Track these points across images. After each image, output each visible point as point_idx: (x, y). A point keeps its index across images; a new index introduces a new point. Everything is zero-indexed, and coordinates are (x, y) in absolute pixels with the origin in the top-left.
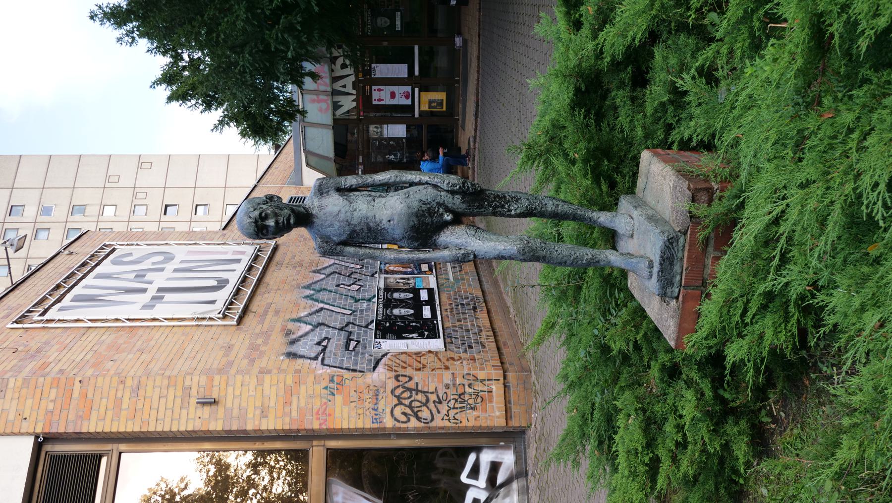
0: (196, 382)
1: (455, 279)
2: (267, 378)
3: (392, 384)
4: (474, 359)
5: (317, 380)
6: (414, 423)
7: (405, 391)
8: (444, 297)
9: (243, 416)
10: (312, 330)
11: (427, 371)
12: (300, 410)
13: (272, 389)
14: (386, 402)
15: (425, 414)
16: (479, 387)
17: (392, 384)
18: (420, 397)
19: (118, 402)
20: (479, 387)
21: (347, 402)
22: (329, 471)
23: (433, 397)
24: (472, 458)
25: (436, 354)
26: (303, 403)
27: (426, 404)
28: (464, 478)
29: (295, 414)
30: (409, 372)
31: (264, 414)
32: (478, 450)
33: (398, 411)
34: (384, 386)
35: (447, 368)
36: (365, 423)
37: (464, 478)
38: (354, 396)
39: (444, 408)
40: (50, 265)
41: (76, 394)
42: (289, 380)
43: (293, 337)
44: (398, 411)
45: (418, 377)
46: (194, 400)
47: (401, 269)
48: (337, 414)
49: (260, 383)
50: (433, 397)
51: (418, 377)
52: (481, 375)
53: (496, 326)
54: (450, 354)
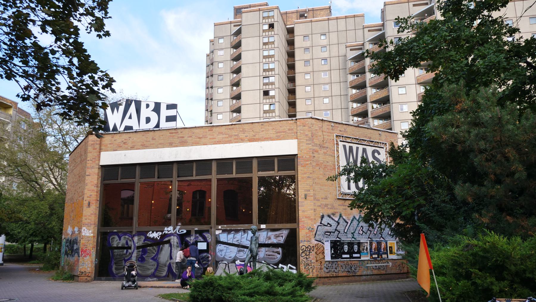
0: (311, 193)
1: (368, 267)
2: (313, 211)
3: (311, 245)
4: (321, 269)
5: (312, 225)
6: (301, 251)
7: (309, 249)
8: (356, 262)
9: (302, 206)
10: (335, 221)
11: (315, 255)
12: (304, 221)
13: (310, 213)
14: (306, 244)
15: (303, 255)
16: (311, 270)
17: (311, 245)
18: (308, 253)
19: (305, 173)
20: (311, 270)
21: (306, 233)
22: (290, 229)
23: (308, 257)
24: (294, 268)
25: (324, 258)
26: (306, 221)
27: (306, 255)
28: (289, 265)
29: (303, 220)
30: (315, 250)
31: (303, 211)
32: (296, 269)
33: (304, 247)
34: (311, 243)
35: (317, 261)
36: (301, 238)
37: (289, 265)
38: (308, 235)
39: (305, 260)
40: (372, 131)
41: (307, 162)
42: (312, 217)
43: (332, 216)
44: (304, 247)
45: (313, 253)
46: (306, 193)
47: (373, 247)
48: (303, 231)
49: (311, 209)
50: (308, 257)
51: (313, 253)
52: (314, 271)
53: (339, 278)
54: (323, 263)
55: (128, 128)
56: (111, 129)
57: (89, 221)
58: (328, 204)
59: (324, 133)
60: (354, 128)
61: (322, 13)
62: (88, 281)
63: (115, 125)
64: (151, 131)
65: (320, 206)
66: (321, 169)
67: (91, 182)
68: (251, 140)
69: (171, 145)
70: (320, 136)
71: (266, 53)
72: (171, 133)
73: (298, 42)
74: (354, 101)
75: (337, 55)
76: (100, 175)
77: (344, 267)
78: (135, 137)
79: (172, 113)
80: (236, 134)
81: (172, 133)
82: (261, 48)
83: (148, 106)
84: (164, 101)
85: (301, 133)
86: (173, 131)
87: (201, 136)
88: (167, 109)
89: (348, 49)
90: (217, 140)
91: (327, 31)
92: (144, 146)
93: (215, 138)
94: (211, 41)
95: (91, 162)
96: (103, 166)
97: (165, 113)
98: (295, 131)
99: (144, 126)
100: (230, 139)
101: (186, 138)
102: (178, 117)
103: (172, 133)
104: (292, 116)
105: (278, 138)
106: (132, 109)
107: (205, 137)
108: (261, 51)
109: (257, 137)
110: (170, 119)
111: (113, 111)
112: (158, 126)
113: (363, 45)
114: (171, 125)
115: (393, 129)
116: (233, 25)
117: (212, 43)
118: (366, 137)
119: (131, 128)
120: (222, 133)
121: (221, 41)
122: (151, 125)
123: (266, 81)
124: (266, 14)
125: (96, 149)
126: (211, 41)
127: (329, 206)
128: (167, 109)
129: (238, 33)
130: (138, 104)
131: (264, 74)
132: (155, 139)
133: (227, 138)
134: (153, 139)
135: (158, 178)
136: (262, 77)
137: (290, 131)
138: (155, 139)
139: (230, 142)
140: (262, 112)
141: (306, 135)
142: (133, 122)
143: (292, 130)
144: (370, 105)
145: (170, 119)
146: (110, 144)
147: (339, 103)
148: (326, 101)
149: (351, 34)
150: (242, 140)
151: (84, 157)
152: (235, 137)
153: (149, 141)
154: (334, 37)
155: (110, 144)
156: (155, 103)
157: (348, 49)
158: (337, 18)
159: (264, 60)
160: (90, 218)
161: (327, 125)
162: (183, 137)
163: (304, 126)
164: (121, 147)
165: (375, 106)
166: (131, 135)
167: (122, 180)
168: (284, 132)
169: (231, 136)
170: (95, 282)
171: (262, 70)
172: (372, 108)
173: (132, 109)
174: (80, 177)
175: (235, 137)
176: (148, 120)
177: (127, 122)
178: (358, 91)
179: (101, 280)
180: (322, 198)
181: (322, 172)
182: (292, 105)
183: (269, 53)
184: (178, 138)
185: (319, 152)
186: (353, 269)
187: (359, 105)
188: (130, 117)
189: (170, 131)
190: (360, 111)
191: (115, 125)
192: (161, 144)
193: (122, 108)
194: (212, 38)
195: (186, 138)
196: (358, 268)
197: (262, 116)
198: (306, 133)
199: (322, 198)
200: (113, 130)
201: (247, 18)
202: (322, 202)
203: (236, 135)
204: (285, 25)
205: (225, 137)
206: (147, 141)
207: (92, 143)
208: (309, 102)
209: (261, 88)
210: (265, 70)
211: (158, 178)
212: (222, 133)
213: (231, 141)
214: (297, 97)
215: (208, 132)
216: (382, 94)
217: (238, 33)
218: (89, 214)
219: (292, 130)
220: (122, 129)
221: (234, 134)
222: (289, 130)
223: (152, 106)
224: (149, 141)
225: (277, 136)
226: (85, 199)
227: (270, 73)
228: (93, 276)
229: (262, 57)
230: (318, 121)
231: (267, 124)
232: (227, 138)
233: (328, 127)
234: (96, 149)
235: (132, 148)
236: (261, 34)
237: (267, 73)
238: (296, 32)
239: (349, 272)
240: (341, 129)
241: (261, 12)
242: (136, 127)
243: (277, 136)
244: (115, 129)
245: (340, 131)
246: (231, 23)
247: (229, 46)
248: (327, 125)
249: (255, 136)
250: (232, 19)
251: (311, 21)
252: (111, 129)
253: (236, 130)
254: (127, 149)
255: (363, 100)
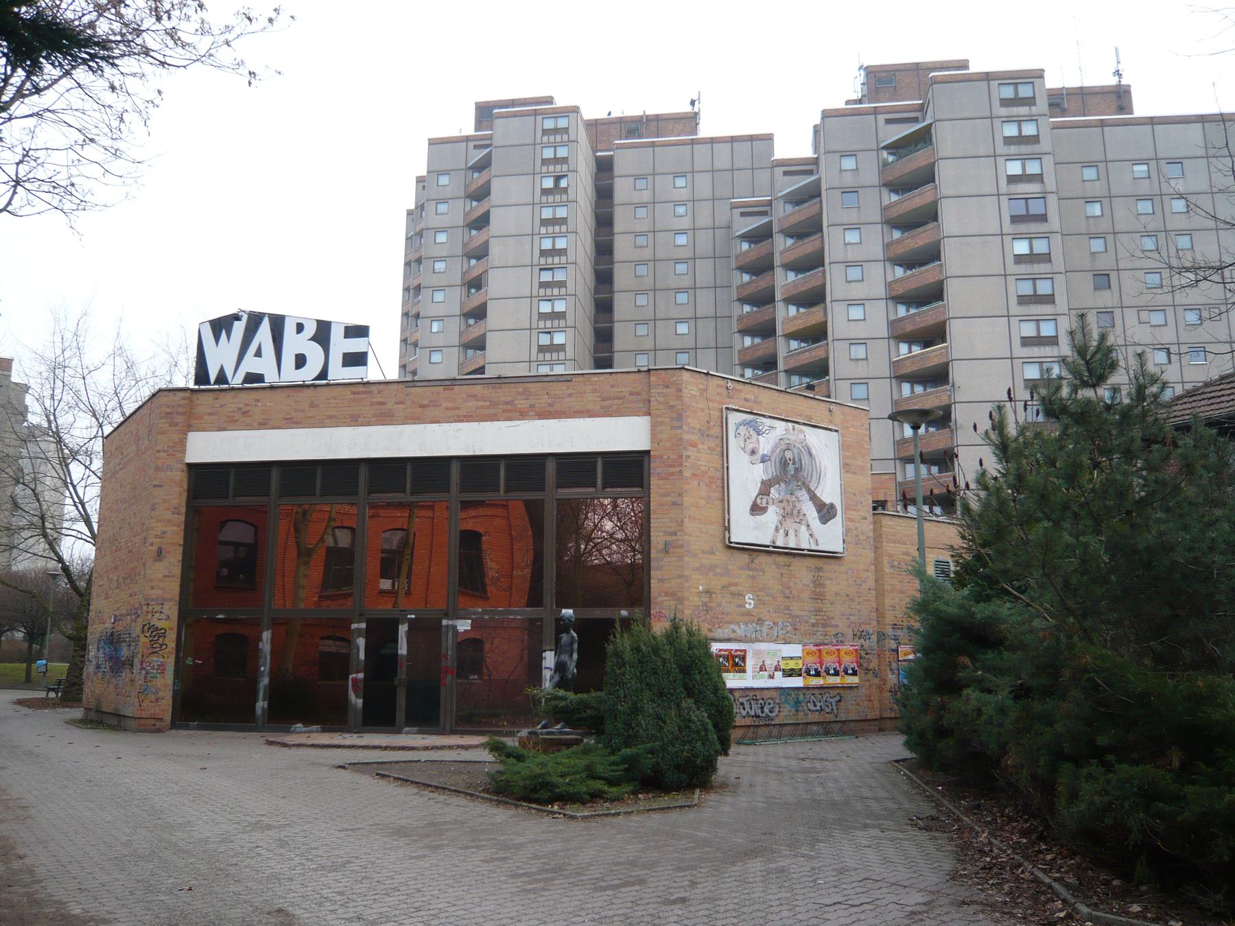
12: (662, 602)
26: (666, 603)
29: (660, 599)
31: (661, 580)
41: (672, 470)
46: (668, 538)
55: (252, 378)
56: (212, 379)
57: (160, 592)
58: (715, 566)
59: (711, 404)
60: (777, 394)
61: (679, 127)
62: (159, 731)
63: (222, 370)
64: (308, 386)
65: (698, 569)
66: (703, 486)
67: (165, 501)
68: (544, 415)
69: (355, 420)
70: (702, 410)
71: (547, 214)
72: (354, 393)
73: (622, 189)
74: (744, 332)
75: (709, 223)
76: (185, 486)
77: (747, 706)
78: (269, 400)
79: (356, 345)
80: (509, 399)
81: (358, 393)
82: (537, 200)
83: (300, 328)
84: (341, 316)
85: (659, 403)
86: (361, 389)
87: (426, 402)
88: (346, 336)
89: (737, 212)
90: (462, 412)
91: (689, 168)
92: (290, 422)
93: (458, 409)
94: (420, 180)
95: (164, 455)
96: (192, 467)
97: (341, 345)
98: (644, 396)
99: (290, 375)
100: (493, 411)
101: (390, 406)
102: (371, 359)
103: (358, 393)
104: (603, 359)
105: (607, 413)
106: (264, 334)
107: (434, 404)
108: (537, 208)
109: (557, 407)
110: (355, 359)
111: (217, 338)
112: (323, 375)
113: (770, 203)
114: (353, 374)
115: (833, 395)
116: (471, 144)
117: (421, 185)
118: (801, 415)
119: (259, 378)
120: (474, 396)
121: (444, 180)
122: (308, 374)
123: (546, 277)
124: (549, 124)
125: (176, 425)
126: (420, 180)
127: (718, 570)
128: (346, 336)
129: (483, 165)
130: (277, 323)
131: (543, 261)
132: (317, 406)
133: (487, 407)
134: (312, 405)
135: (412, 494)
136: (536, 269)
137: (634, 398)
138: (317, 406)
139: (493, 418)
140: (535, 349)
141: (672, 407)
142: (265, 366)
143: (638, 394)
144: (781, 341)
145: (355, 359)
146: (210, 414)
147: (712, 334)
148: (683, 329)
149: (743, 178)
150: (523, 415)
151: (146, 441)
152: (505, 407)
153: (303, 411)
154: (703, 181)
155: (210, 414)
156: (318, 322)
157: (737, 212)
158: (713, 141)
159: (543, 230)
160: (161, 584)
161: (718, 386)
162: (383, 403)
163: (667, 387)
164: (236, 421)
165: (794, 344)
166: (261, 394)
167: (242, 500)
168: (618, 398)
169: (495, 404)
170: (174, 732)
171: (537, 253)
172: (787, 350)
173: (264, 334)
174: (135, 489)
175: (505, 407)
176: (301, 361)
177: (251, 364)
178: (755, 309)
179: (187, 728)
180: (703, 552)
181: (703, 493)
182: (603, 337)
183: (554, 212)
184: (372, 404)
185: (700, 446)
186: (766, 710)
187: (757, 340)
188: (258, 354)
189: (354, 389)
190: (760, 353)
191: (222, 370)
192: (331, 417)
193: (239, 328)
194: (423, 172)
195: (390, 406)
196: (777, 710)
197: (534, 358)
198: (671, 403)
199: (703, 552)
200: (216, 382)
201: (503, 131)
202: (704, 561)
203: (507, 403)
204: (595, 150)
205: (483, 407)
206: (296, 410)
207: (168, 410)
208: (642, 330)
209: (535, 293)
210: (544, 253)
211: (412, 494)
212: (474, 396)
213: (495, 415)
214: (617, 316)
215: (411, 396)
216: (811, 317)
217: (483, 165)
218: (160, 576)
219: (638, 394)
220: (236, 381)
221: (504, 399)
222: (631, 394)
223: (310, 330)
224: (303, 411)
225: (602, 407)
226: (150, 541)
227: (557, 260)
228: (168, 717)
229: (537, 222)
230: (697, 376)
231: (581, 379)
232: (487, 407)
233: (719, 390)
234: (176, 425)
235: (263, 425)
236: (538, 169)
237: (550, 260)
238: (618, 169)
239: (757, 716)
240: (748, 397)
241: (539, 118)
242: (271, 377)
243: (602, 407)
244: (222, 378)
245: (746, 400)
246: (467, 139)
247: (463, 194)
248: (718, 386)
249: (551, 405)
250: (469, 130)
251: (653, 144)
252: (213, 378)
253: (480, 391)
254: (249, 427)
255: (766, 331)
